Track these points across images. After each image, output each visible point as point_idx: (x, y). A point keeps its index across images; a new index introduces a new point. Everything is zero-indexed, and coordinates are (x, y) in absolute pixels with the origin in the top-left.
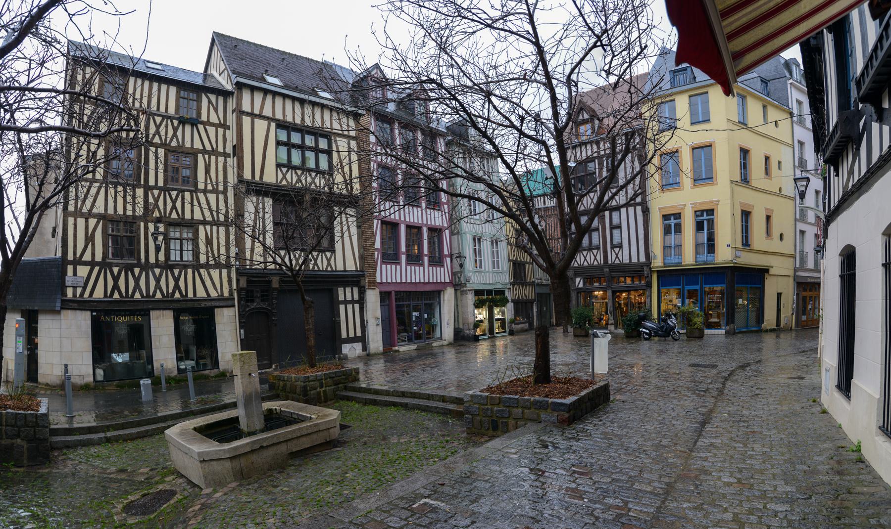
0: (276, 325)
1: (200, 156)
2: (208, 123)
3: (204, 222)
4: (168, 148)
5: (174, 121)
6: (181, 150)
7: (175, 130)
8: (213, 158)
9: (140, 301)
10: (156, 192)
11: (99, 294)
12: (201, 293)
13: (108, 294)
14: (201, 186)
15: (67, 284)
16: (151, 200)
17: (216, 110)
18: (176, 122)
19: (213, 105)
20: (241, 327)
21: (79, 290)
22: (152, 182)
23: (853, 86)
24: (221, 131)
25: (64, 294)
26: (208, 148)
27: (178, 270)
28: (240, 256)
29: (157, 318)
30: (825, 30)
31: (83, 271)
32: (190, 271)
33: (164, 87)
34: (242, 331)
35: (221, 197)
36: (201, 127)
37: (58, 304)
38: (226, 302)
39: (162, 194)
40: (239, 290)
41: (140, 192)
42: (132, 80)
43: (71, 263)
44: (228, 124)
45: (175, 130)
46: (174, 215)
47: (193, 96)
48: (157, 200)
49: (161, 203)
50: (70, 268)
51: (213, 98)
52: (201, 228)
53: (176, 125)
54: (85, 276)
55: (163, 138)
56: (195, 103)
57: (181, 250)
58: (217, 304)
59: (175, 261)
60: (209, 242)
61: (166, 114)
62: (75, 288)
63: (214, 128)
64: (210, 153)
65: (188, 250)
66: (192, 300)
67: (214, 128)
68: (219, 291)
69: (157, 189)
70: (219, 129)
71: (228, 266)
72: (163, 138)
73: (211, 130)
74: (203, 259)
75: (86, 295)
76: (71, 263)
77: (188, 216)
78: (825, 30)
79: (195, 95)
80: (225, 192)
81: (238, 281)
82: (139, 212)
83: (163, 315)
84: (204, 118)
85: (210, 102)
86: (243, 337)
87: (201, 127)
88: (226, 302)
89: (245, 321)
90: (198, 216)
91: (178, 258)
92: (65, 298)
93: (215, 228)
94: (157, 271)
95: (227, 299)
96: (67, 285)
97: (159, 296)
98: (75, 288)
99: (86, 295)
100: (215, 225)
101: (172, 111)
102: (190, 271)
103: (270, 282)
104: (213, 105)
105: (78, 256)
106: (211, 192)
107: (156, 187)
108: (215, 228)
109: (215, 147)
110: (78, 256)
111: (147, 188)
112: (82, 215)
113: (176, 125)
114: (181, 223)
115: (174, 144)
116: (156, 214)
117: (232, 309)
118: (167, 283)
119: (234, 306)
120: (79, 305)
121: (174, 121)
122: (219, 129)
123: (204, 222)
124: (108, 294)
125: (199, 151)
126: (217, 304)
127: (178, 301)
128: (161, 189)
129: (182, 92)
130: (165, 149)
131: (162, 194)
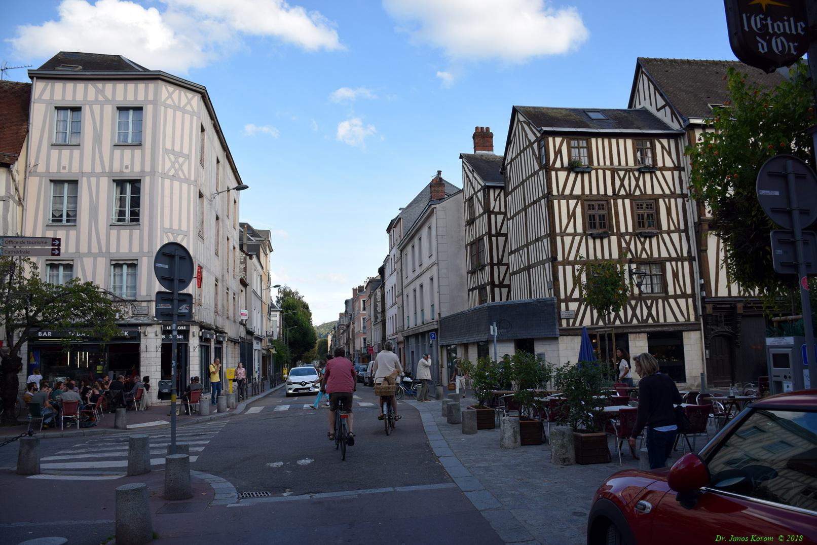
0: (739, 347)
1: (661, 201)
2: (664, 168)
3: (670, 259)
4: (632, 198)
5: (635, 172)
6: (644, 198)
7: (637, 180)
8: (673, 200)
9: (620, 327)
10: (627, 238)
11: (587, 322)
12: (671, 319)
13: (595, 322)
14: (665, 227)
15: (562, 317)
16: (624, 245)
17: (669, 154)
18: (637, 174)
19: (666, 150)
20: (706, 348)
21: (571, 321)
22: (623, 230)
23: (576, 271)
24: (676, 173)
25: (561, 325)
26: (667, 192)
27: (650, 301)
28: (705, 287)
29: (634, 340)
30: (571, 325)
31: (573, 306)
32: (660, 301)
33: (621, 141)
34: (707, 352)
35: (683, 235)
36: (658, 173)
37: (558, 333)
38: (691, 327)
39: (633, 239)
40: (705, 316)
41: (614, 239)
42: (593, 140)
43: (563, 301)
44: (682, 166)
45: (637, 180)
46: (644, 256)
47: (583, 143)
48: (628, 244)
49: (632, 247)
50: (563, 305)
51: (665, 142)
52: (668, 264)
53: (637, 176)
54: (576, 309)
55: (628, 189)
56: (585, 150)
57: (652, 284)
58: (684, 328)
59: (647, 293)
60: (675, 275)
61: (605, 167)
62: (568, 320)
63: (670, 172)
64: (669, 197)
65: (657, 284)
66: (662, 326)
67: (670, 172)
68: (686, 316)
69: (627, 235)
70: (674, 172)
71: (693, 295)
72: (628, 189)
73: (668, 174)
74: (671, 291)
75: (577, 324)
76: (563, 301)
77: (656, 255)
78: (571, 325)
79: (585, 142)
80: (686, 231)
81: (704, 308)
82: (615, 255)
83: (639, 338)
84: (660, 164)
85: (663, 147)
86: (708, 357)
87: (658, 173)
88: (691, 327)
89: (709, 343)
90: (664, 254)
91: (649, 291)
92: (562, 328)
93: (680, 263)
94: (633, 302)
95: (693, 324)
96: (562, 318)
97: (635, 322)
98: (568, 320)
99: (577, 324)
100: (679, 260)
101: (631, 163)
102: (660, 301)
103: (735, 307)
104: (666, 150)
105: (568, 294)
106: (673, 232)
107: (627, 233)
108: (680, 263)
109: (673, 190)
110: (568, 294)
111: (620, 236)
112: (569, 263)
113: (637, 176)
114: (650, 262)
115: (638, 193)
116: (629, 256)
117: (699, 332)
118: (642, 311)
119: (700, 330)
120: (570, 332)
121: (635, 172)
122: (674, 172)
123: (670, 259)
124: (595, 322)
125: (660, 196)
126: (684, 328)
127: (651, 326)
128: (631, 235)
129: (572, 142)
130: (630, 200)
131: (633, 239)
